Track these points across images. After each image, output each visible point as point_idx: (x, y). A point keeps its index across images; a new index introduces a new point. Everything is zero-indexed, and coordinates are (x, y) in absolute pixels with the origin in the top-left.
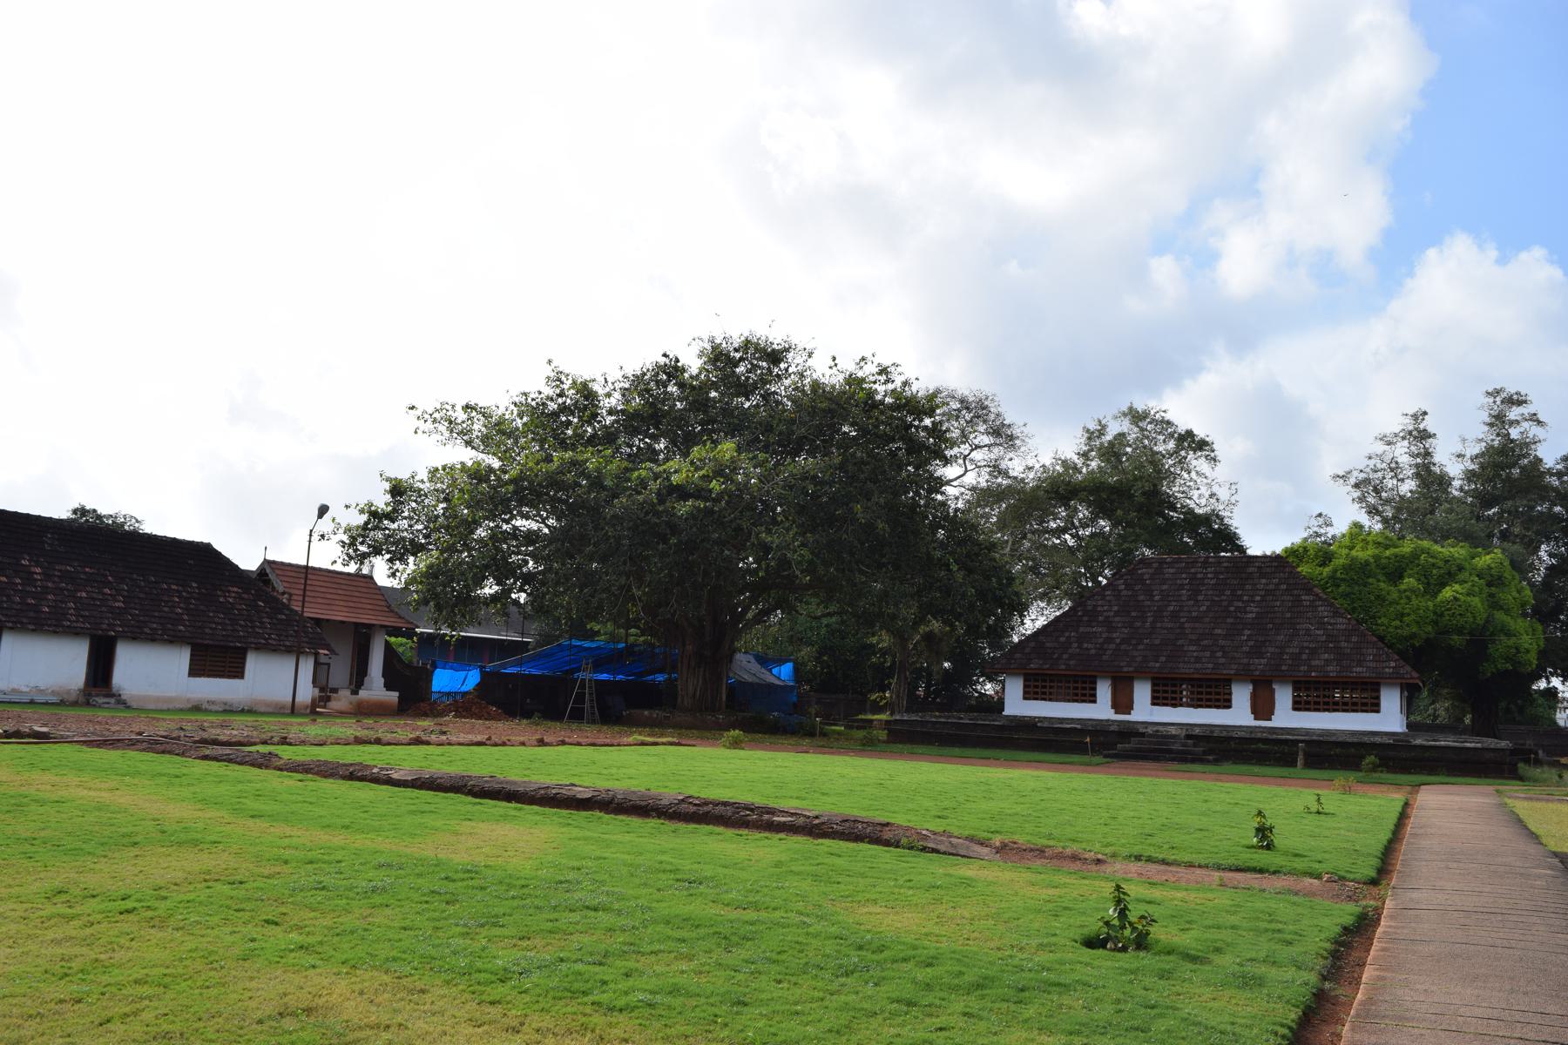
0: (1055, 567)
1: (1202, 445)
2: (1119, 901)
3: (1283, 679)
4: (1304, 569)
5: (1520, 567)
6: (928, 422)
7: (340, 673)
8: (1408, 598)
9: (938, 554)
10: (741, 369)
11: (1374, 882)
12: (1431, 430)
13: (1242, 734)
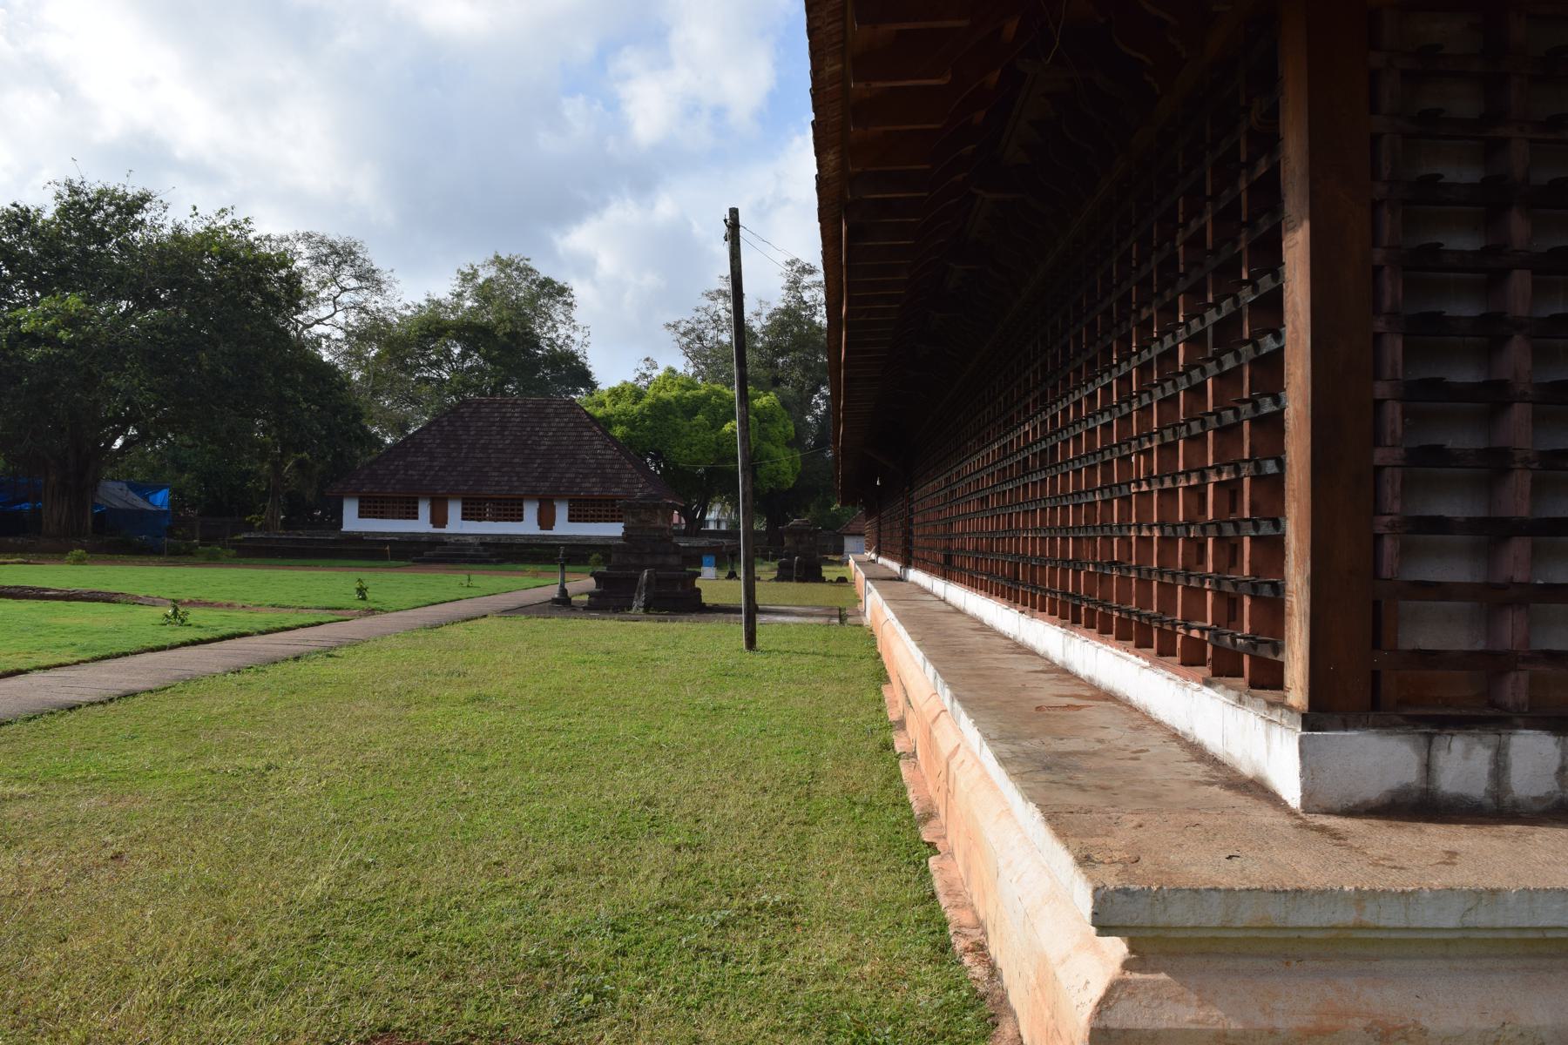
1: (562, 291)
3: (561, 498)
6: (283, 273)
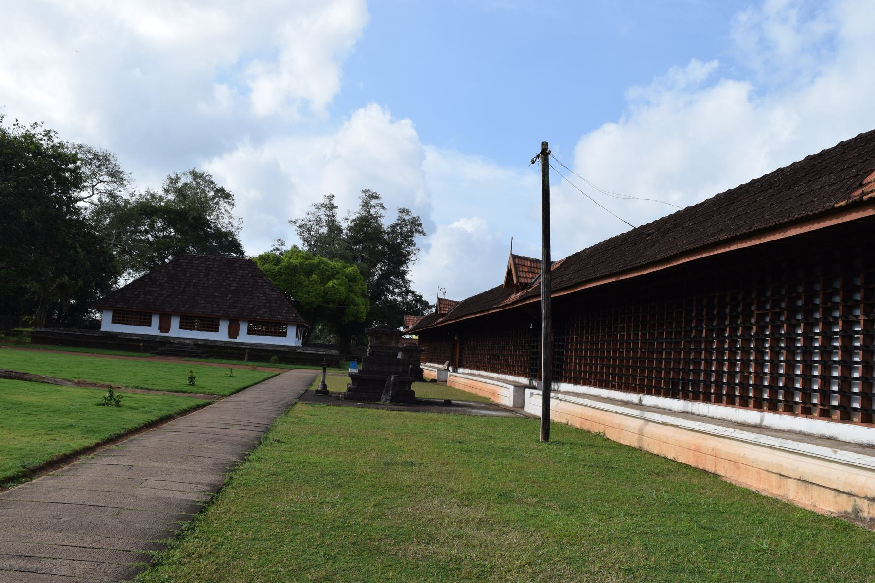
1: (228, 196)
3: (244, 319)
5: (366, 274)
6: (71, 166)
9: (70, 241)
12: (335, 204)
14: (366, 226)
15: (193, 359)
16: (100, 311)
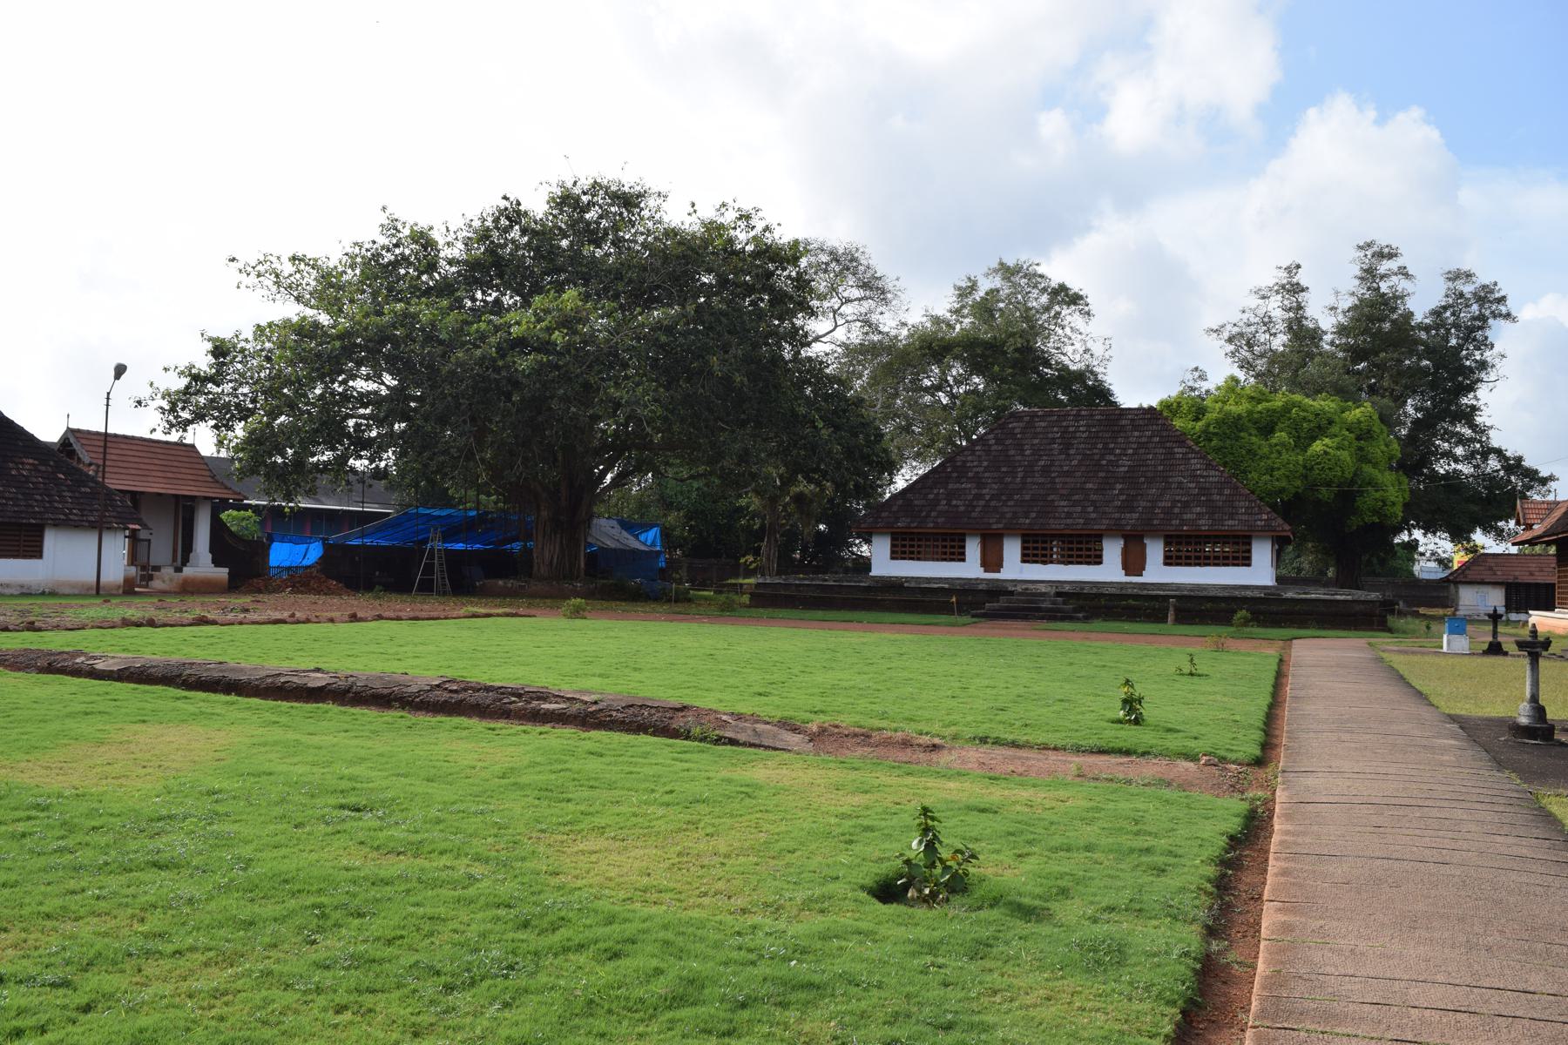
0: (928, 428)
1: (1075, 299)
2: (926, 830)
3: (1154, 533)
4: (1178, 423)
5: (1388, 420)
7: (161, 548)
8: (1279, 453)
10: (591, 215)
11: (1259, 762)
12: (1304, 283)
13: (1113, 591)
14: (1376, 318)
15: (1060, 625)
16: (868, 542)
